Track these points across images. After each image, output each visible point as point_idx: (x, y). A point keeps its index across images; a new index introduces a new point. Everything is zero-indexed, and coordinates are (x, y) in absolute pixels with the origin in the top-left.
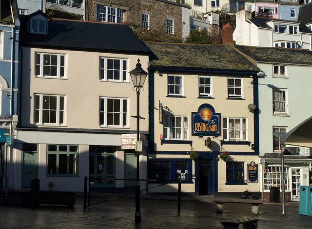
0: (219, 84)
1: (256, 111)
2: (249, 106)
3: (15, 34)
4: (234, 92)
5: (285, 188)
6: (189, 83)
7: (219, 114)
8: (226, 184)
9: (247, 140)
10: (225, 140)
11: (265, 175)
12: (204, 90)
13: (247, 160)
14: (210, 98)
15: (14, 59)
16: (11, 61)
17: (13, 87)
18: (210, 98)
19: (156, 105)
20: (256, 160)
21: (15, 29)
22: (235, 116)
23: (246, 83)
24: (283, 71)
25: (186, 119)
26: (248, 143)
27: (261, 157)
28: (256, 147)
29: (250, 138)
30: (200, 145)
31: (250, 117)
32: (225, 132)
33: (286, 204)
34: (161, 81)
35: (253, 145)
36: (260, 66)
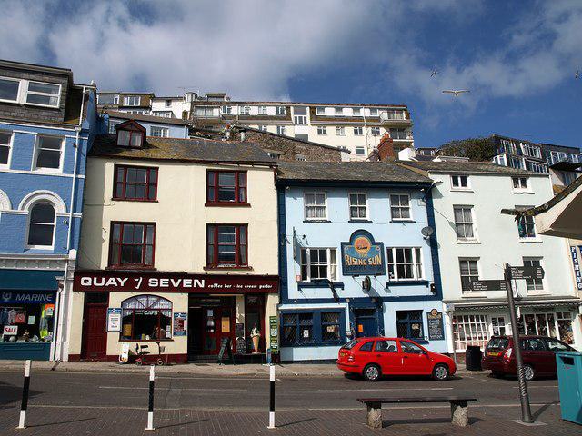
0: (378, 207)
1: (433, 244)
2: (423, 231)
3: (81, 140)
4: (399, 216)
5: (210, 346)
6: (337, 206)
7: (381, 244)
8: (112, 199)
9: (424, 278)
10: (392, 280)
11: (454, 327)
12: (357, 213)
13: (426, 307)
14: (366, 222)
15: (78, 173)
16: (73, 176)
17: (74, 211)
18: (366, 222)
19: (290, 237)
20: (439, 306)
21: (82, 133)
22: (403, 244)
23: (416, 208)
24: (464, 184)
25: (333, 251)
26: (425, 283)
27: (446, 302)
28: (437, 293)
29: (427, 275)
30: (353, 288)
31: (426, 251)
32: (391, 268)
33: (104, 265)
34: (295, 205)
35: (432, 285)
36: (435, 178)
